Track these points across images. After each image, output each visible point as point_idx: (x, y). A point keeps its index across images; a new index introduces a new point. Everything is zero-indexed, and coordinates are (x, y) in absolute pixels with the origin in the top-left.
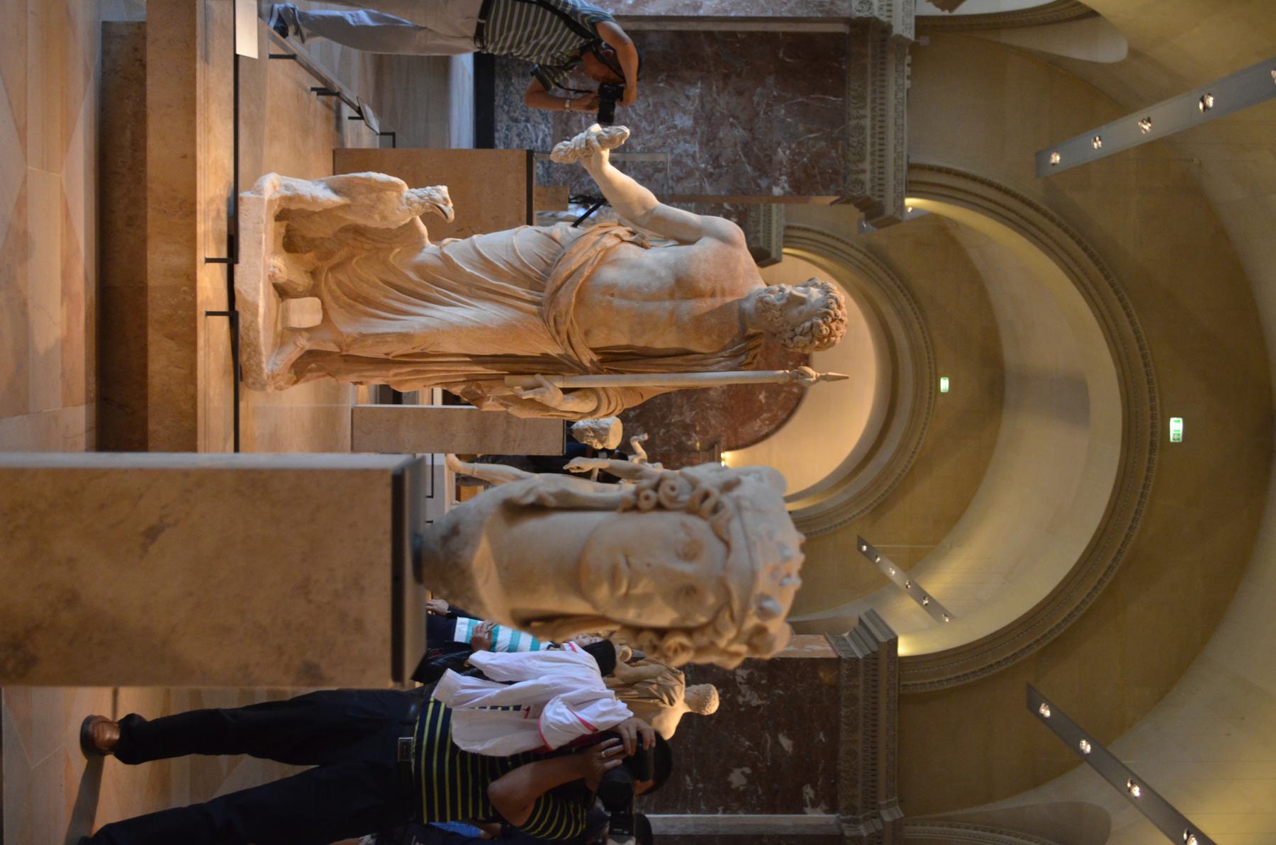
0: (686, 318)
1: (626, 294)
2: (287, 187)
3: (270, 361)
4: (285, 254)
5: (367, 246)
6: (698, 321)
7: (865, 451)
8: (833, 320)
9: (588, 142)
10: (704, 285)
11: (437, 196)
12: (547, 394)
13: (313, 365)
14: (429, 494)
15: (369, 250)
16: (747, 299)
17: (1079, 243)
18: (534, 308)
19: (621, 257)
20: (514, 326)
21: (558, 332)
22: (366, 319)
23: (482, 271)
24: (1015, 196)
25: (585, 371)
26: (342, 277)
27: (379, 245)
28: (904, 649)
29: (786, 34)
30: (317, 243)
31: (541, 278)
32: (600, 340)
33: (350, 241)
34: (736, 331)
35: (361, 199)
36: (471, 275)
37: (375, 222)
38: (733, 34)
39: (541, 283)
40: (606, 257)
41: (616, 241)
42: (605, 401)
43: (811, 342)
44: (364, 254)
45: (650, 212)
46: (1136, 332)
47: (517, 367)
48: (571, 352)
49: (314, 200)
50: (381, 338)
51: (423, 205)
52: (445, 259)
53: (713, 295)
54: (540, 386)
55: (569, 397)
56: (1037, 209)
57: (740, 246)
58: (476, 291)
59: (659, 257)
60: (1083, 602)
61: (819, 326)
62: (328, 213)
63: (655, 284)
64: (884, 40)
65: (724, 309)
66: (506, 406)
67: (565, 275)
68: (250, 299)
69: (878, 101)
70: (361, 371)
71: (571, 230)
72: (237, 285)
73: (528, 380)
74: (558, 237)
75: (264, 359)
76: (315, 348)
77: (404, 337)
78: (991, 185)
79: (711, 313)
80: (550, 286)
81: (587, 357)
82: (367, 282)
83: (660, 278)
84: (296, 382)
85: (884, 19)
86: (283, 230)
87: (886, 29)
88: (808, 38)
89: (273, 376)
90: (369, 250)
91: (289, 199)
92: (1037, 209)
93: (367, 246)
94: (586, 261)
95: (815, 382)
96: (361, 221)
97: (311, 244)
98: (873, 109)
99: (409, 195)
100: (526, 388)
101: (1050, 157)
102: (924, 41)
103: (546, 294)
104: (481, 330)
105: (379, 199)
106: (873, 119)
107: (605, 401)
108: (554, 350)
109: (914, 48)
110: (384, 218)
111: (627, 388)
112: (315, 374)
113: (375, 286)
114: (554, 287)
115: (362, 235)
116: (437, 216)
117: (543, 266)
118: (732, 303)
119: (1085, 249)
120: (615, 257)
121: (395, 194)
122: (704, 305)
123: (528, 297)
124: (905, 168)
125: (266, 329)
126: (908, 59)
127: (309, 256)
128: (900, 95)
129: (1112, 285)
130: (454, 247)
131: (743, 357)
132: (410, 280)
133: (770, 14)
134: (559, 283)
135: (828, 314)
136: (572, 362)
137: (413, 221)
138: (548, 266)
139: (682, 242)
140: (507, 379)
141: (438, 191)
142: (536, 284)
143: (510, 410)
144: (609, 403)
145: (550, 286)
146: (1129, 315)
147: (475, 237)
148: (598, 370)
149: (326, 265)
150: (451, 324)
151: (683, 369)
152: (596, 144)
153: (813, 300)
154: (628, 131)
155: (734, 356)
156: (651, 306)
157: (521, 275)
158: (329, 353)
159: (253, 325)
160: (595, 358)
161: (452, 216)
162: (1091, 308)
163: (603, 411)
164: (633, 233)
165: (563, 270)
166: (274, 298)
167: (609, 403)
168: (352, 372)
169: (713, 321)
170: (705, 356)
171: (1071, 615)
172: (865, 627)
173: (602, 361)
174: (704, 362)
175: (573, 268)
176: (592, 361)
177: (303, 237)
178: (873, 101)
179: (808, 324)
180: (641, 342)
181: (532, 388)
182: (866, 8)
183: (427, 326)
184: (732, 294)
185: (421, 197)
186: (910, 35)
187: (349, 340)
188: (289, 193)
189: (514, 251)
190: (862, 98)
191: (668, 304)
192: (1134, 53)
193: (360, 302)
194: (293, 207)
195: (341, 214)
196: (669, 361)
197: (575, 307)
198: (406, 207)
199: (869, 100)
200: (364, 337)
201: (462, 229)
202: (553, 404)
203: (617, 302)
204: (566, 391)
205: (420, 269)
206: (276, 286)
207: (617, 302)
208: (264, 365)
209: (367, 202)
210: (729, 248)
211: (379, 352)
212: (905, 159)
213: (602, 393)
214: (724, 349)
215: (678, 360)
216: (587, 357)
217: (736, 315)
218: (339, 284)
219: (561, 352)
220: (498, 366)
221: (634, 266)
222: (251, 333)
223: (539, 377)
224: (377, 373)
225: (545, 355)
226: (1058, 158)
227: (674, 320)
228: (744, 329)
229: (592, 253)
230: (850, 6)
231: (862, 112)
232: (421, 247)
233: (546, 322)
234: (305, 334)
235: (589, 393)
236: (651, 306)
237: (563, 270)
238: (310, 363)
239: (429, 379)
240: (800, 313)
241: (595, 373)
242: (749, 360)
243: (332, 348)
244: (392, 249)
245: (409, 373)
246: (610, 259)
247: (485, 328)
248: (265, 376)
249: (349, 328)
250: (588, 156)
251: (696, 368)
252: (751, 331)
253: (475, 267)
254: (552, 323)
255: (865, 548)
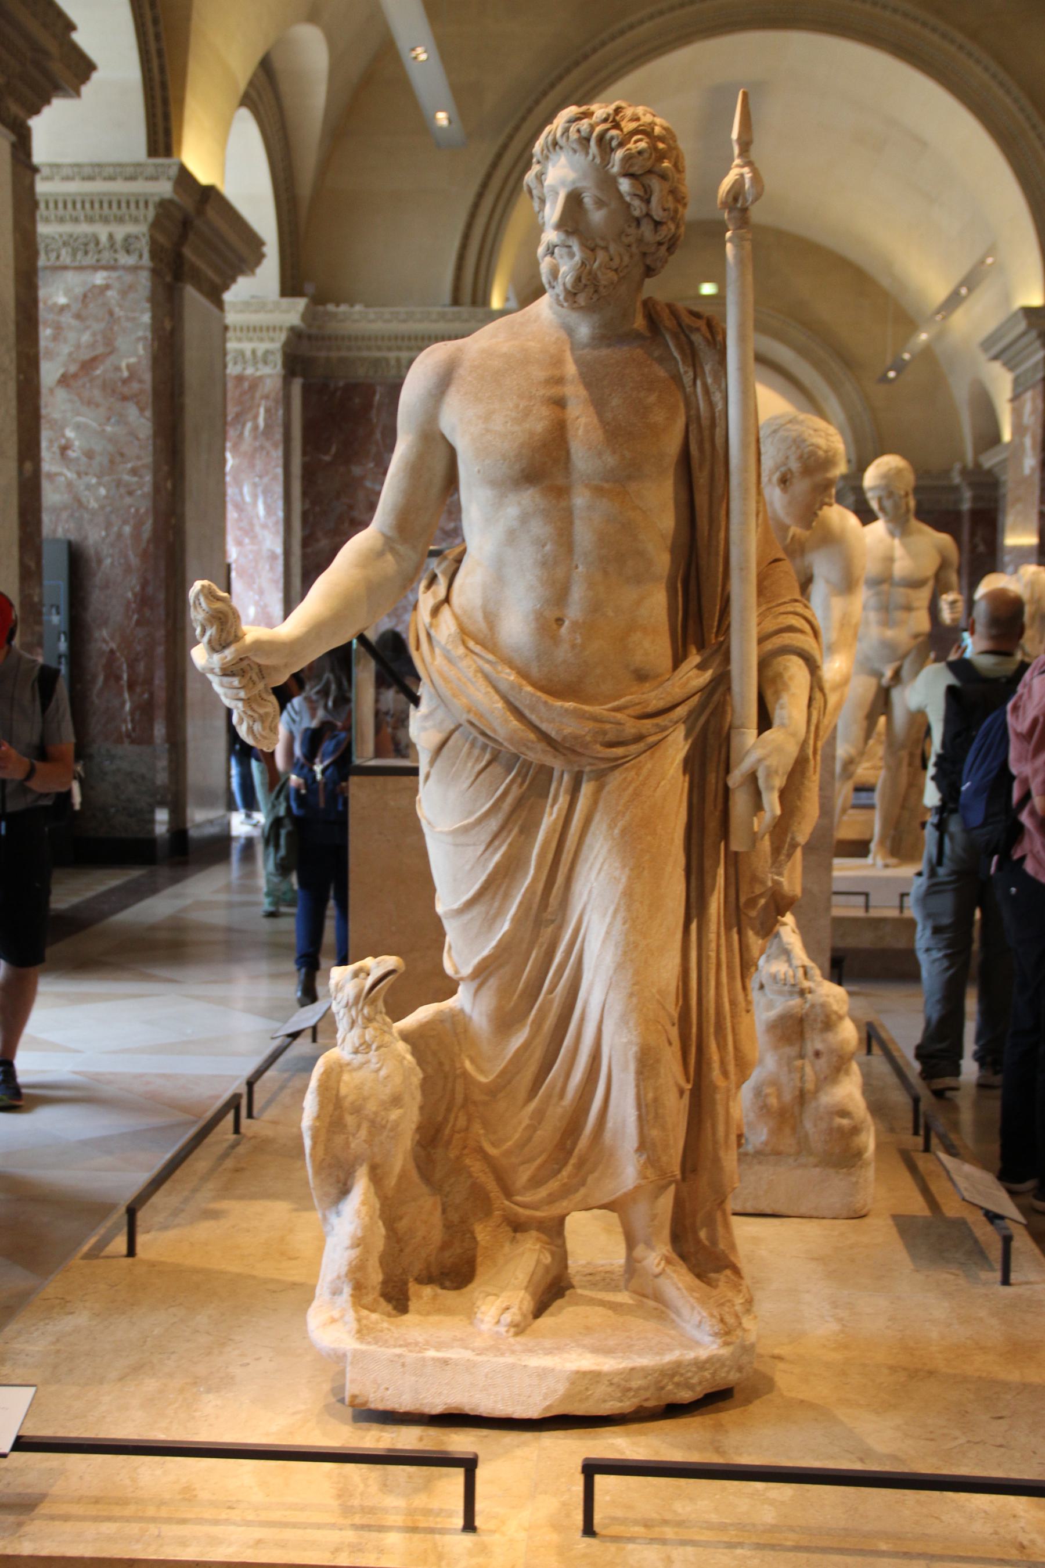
0: (611, 460)
1: (558, 594)
2: (336, 1292)
3: (690, 1338)
4: (474, 1289)
5: (462, 1122)
6: (615, 433)
7: (779, 380)
8: (617, 126)
9: (227, 672)
10: (539, 423)
11: (350, 990)
12: (773, 762)
13: (703, 1234)
14: (861, 899)
15: (470, 1120)
16: (570, 331)
17: (545, 94)
18: (586, 789)
19: (478, 602)
20: (624, 832)
21: (639, 738)
22: (608, 1135)
23: (507, 897)
24: (489, 176)
25: (722, 682)
26: (524, 1176)
27: (459, 1098)
28: (1035, 300)
29: (304, 453)
30: (455, 1217)
31: (522, 775)
32: (655, 646)
33: (452, 1155)
34: (639, 352)
35: (358, 1142)
36: (517, 921)
37: (407, 1119)
38: (305, 515)
39: (535, 776)
40: (479, 637)
41: (446, 612)
42: (788, 639)
43: (663, 176)
44: (477, 1128)
45: (389, 544)
46: (651, 17)
47: (712, 824)
48: (681, 711)
49: (360, 1242)
50: (648, 1111)
51: (369, 1020)
52: (482, 972)
53: (560, 403)
54: (752, 777)
55: (778, 715)
56: (505, 147)
57: (460, 350)
58: (548, 911)
59: (486, 521)
60: (986, 69)
61: (628, 159)
62: (389, 1210)
63: (538, 528)
64: (310, 337)
65: (591, 377)
66: (794, 846)
67: (515, 723)
68: (561, 1388)
69: (379, 343)
70: (715, 1142)
71: (424, 707)
72: (534, 1412)
73: (740, 802)
74: (436, 738)
75: (690, 1355)
76: (666, 1233)
77: (646, 1064)
78: (476, 206)
79: (599, 404)
80: (539, 755)
81: (693, 677)
82: (532, 1128)
83: (524, 519)
84: (736, 1271)
85: (283, 337)
86: (428, 1291)
87: (296, 335)
88: (310, 429)
89: (726, 1332)
90: (470, 1120)
91: (359, 1288)
92: (505, 147)
93: (462, 1122)
94: (487, 677)
95: (755, 171)
96: (407, 1140)
97: (458, 1230)
98: (389, 349)
99: (348, 1047)
100: (758, 806)
101: (441, 128)
102: (310, 288)
103: (557, 764)
104: (635, 905)
105: (357, 1110)
106: (399, 349)
107: (788, 639)
108: (677, 746)
109: (318, 300)
110: (396, 1101)
111: (761, 591)
112: (720, 1230)
113: (539, 1116)
114: (541, 746)
115: (439, 1130)
116: (392, 988)
117: (497, 769)
118: (578, 362)
119: (552, 86)
120: (479, 616)
121: (346, 1077)
122: (582, 420)
123: (563, 800)
124: (456, 309)
125: (628, 1349)
126: (331, 307)
127: (482, 1233)
128: (372, 316)
129: (595, 50)
130: (460, 956)
131: (696, 338)
132: (526, 1046)
133: (280, 471)
134: (532, 736)
135: (601, 138)
136: (702, 706)
137: (406, 1037)
138: (497, 756)
139: (451, 481)
140: (734, 847)
141: (339, 988)
142: (534, 786)
143: (802, 838)
144: (791, 629)
145: (539, 755)
146: (632, 27)
147: (440, 908)
148: (720, 655)
149: (500, 1202)
150: (619, 967)
151: (720, 470)
152: (229, 653)
153: (571, 175)
154: (198, 585)
155: (693, 358)
156: (584, 535)
157: (518, 814)
158: (679, 1203)
159: (621, 1382)
160: (695, 659)
161: (390, 962)
162: (627, 73)
163: (806, 642)
164: (433, 580)
165: (504, 726)
166: (563, 1315)
167: (791, 629)
168: (716, 1160)
169: (615, 402)
170: (692, 420)
171: (1001, 84)
172: (1003, 351)
173: (701, 647)
174: (705, 422)
175: (500, 705)
176: (701, 667)
177: (445, 1246)
178: (379, 349)
179: (625, 185)
180: (662, 561)
181: (757, 794)
182: (271, 358)
183: (624, 1019)
184: (557, 362)
185: (353, 1023)
186: (301, 303)
187: (650, 1172)
188: (347, 1290)
189: (466, 830)
190: (376, 363)
191: (580, 500)
192: (313, 17)
193: (573, 1146)
194: (376, 1277)
195: (392, 1181)
196: (702, 500)
197: (586, 702)
198: (373, 1055)
199: (378, 354)
200: (643, 1145)
201: (423, 937)
202: (792, 750)
203: (574, 611)
204: (765, 722)
205: (505, 1022)
206: (540, 1310)
207: (574, 611)
208: (703, 1354)
209: (363, 1133)
210: (461, 371)
211: (676, 1109)
212: (447, 309)
213: (770, 645)
214: (677, 378)
215: (701, 479)
216: (693, 677)
217: (604, 352)
218: (536, 1182)
219: (680, 731)
220: (708, 864)
221: (499, 578)
222: (635, 1384)
223: (735, 778)
224: (720, 1110)
225: (688, 764)
226: (423, 57)
227: (619, 483)
228: (638, 336)
229: (467, 666)
230: (270, 376)
231: (393, 362)
232: (457, 1020)
233: (616, 764)
234: (640, 1251)
235: (770, 673)
236: (584, 535)
237: (504, 726)
238: (698, 1241)
239: (733, 1003)
240: (600, 203)
241: (727, 659)
242: (701, 324)
243: (666, 1202)
244: (465, 1074)
245: (722, 1047)
246: (482, 625)
247: (628, 894)
248: (725, 1351)
249: (628, 1171)
250: (262, 672)
251: (719, 441)
252: (639, 322)
253: (500, 913)
254: (619, 751)
255: (892, 374)
